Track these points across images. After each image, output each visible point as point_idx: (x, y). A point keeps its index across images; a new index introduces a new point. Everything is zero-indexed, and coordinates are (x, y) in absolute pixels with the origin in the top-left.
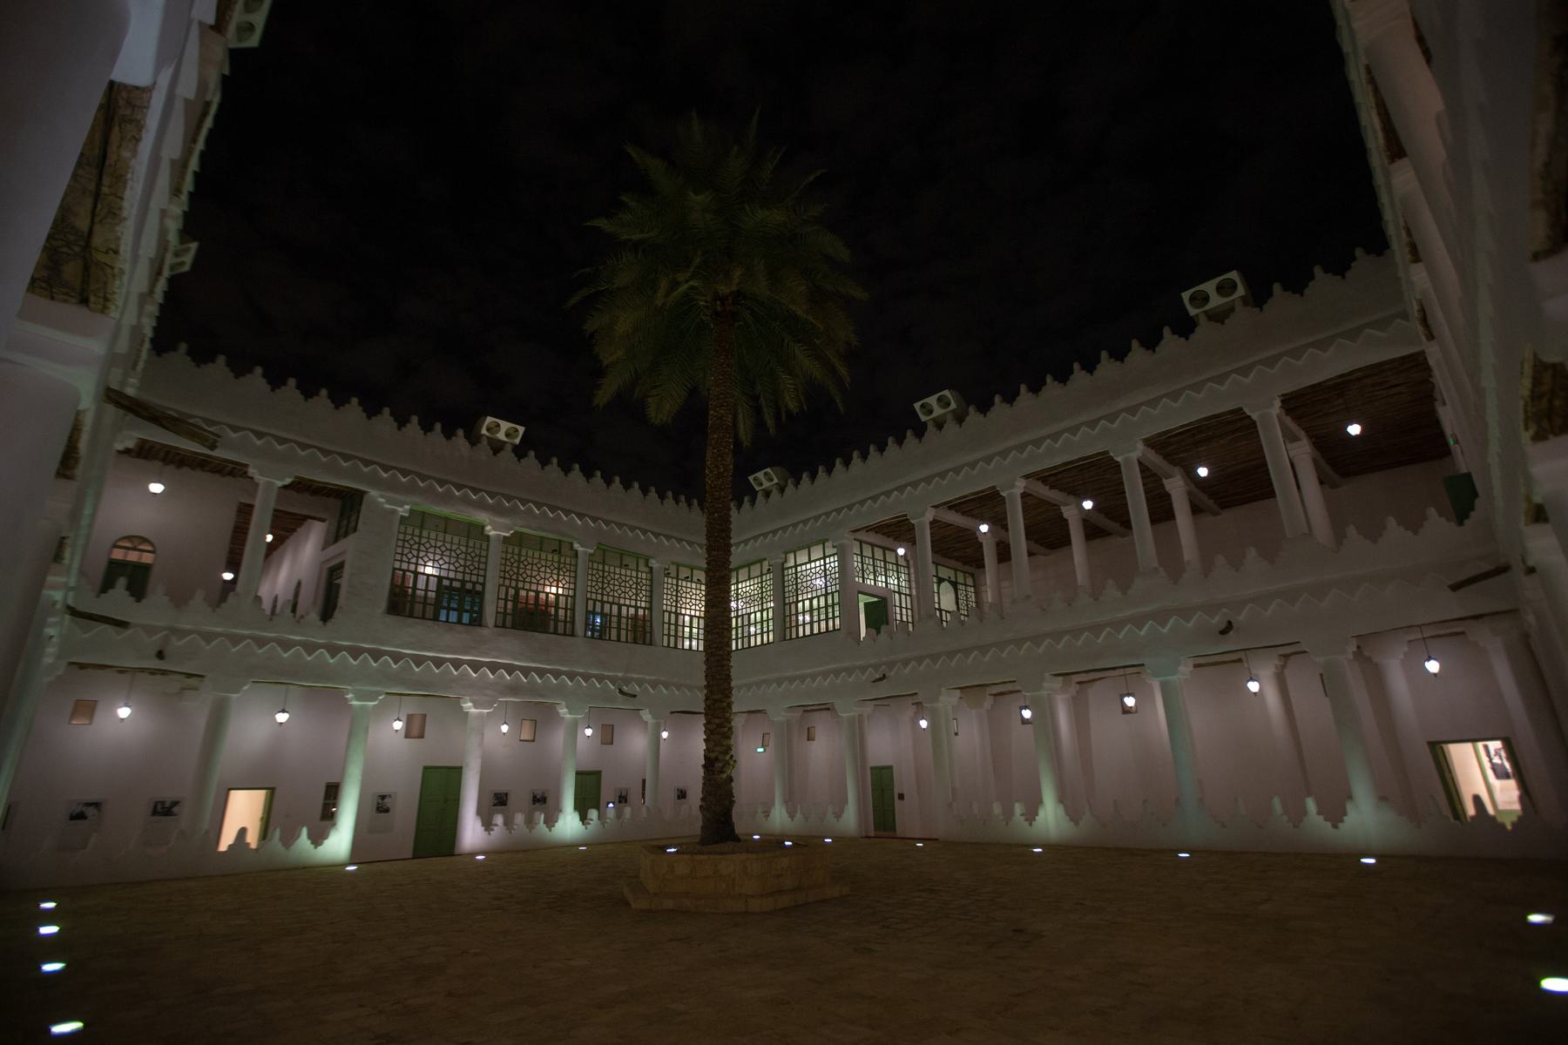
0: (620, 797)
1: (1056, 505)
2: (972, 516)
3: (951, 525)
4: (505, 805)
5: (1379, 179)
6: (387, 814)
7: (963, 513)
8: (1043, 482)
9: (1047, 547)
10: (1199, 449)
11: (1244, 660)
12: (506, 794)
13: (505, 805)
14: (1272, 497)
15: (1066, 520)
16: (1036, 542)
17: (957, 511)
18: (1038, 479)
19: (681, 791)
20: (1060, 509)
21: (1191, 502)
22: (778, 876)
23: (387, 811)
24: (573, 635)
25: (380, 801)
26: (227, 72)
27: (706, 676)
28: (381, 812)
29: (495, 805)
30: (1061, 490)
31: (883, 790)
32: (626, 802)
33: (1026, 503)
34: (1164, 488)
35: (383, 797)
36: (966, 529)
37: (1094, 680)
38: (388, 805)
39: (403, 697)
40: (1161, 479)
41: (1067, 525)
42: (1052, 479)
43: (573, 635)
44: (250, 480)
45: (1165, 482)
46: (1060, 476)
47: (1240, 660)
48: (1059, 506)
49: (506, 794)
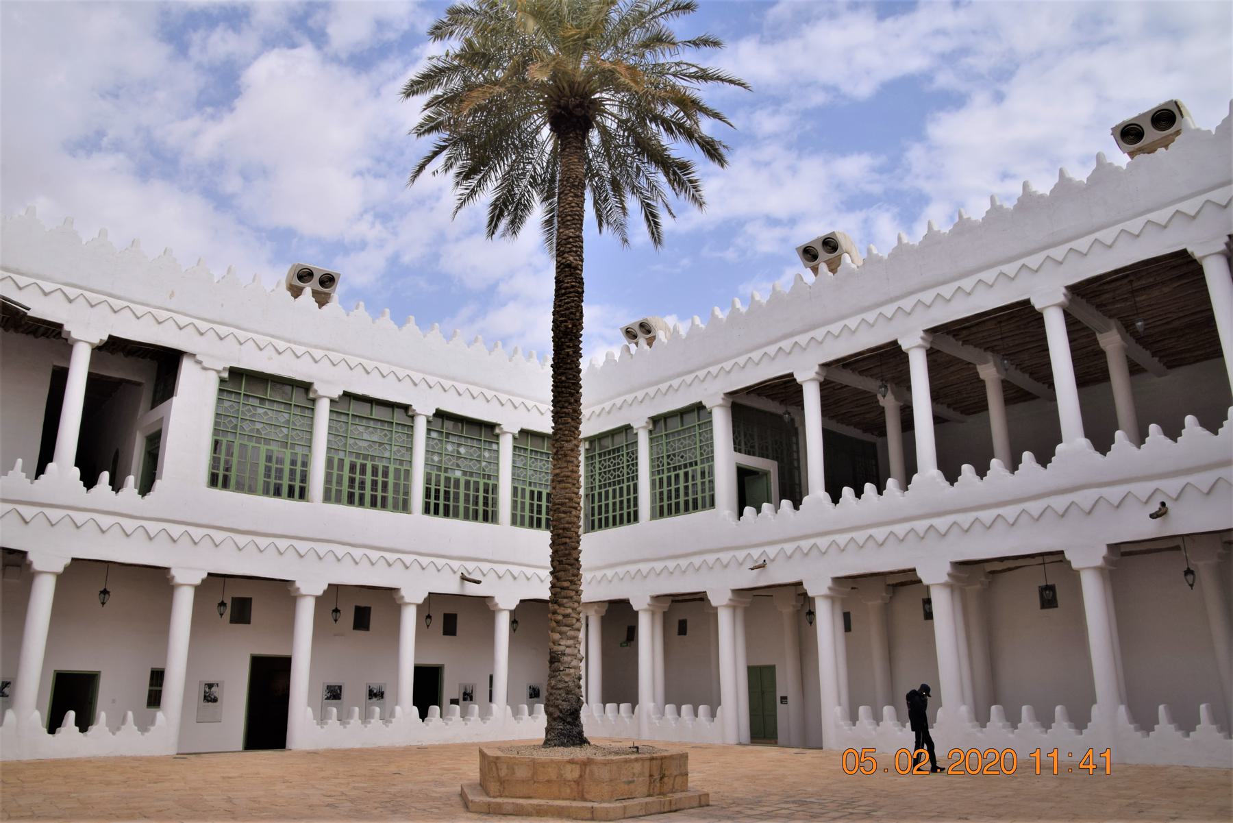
0: (465, 694)
1: (970, 363)
2: (871, 376)
3: (847, 386)
4: (340, 699)
5: (141, 411)
6: (214, 704)
7: (861, 373)
8: (954, 336)
9: (962, 412)
10: (1138, 299)
11: (1182, 547)
12: (340, 687)
13: (340, 699)
14: (1207, 357)
15: (983, 381)
16: (949, 406)
17: (853, 370)
18: (948, 333)
19: (534, 689)
20: (976, 369)
21: (1127, 356)
22: (630, 782)
23: (215, 700)
24: (303, 495)
25: (207, 690)
26: (30, 313)
27: (552, 561)
28: (208, 701)
29: (328, 698)
30: (975, 346)
31: (763, 693)
32: (471, 700)
33: (935, 361)
34: (1098, 344)
35: (210, 686)
36: (869, 392)
37: (1010, 569)
38: (216, 695)
39: (227, 579)
40: (1094, 333)
41: (984, 387)
42: (965, 333)
43: (303, 495)
44: (64, 340)
45: (1099, 336)
46: (974, 330)
47: (1178, 548)
48: (975, 365)
49: (340, 687)
